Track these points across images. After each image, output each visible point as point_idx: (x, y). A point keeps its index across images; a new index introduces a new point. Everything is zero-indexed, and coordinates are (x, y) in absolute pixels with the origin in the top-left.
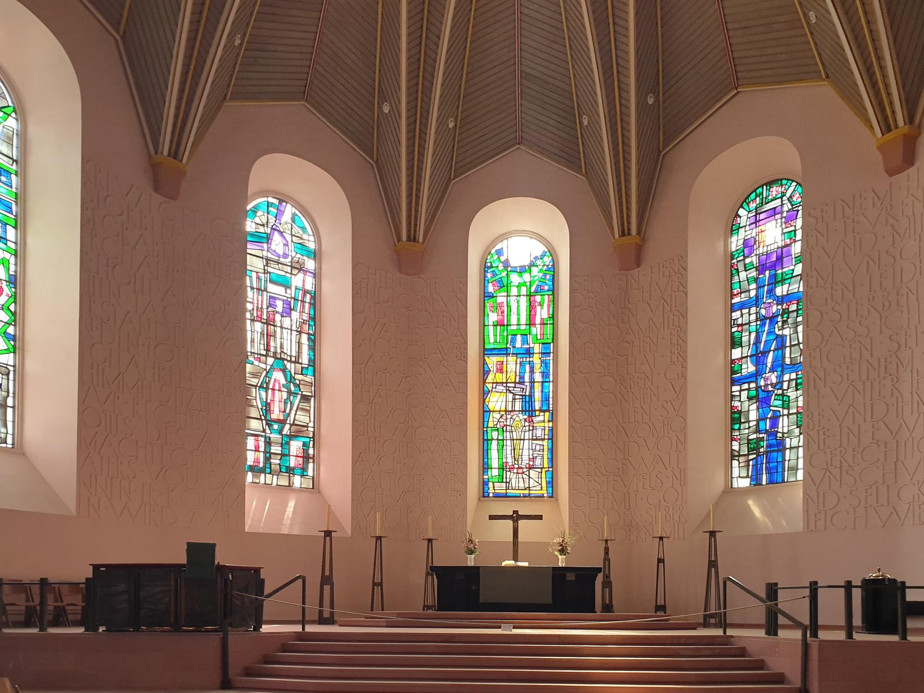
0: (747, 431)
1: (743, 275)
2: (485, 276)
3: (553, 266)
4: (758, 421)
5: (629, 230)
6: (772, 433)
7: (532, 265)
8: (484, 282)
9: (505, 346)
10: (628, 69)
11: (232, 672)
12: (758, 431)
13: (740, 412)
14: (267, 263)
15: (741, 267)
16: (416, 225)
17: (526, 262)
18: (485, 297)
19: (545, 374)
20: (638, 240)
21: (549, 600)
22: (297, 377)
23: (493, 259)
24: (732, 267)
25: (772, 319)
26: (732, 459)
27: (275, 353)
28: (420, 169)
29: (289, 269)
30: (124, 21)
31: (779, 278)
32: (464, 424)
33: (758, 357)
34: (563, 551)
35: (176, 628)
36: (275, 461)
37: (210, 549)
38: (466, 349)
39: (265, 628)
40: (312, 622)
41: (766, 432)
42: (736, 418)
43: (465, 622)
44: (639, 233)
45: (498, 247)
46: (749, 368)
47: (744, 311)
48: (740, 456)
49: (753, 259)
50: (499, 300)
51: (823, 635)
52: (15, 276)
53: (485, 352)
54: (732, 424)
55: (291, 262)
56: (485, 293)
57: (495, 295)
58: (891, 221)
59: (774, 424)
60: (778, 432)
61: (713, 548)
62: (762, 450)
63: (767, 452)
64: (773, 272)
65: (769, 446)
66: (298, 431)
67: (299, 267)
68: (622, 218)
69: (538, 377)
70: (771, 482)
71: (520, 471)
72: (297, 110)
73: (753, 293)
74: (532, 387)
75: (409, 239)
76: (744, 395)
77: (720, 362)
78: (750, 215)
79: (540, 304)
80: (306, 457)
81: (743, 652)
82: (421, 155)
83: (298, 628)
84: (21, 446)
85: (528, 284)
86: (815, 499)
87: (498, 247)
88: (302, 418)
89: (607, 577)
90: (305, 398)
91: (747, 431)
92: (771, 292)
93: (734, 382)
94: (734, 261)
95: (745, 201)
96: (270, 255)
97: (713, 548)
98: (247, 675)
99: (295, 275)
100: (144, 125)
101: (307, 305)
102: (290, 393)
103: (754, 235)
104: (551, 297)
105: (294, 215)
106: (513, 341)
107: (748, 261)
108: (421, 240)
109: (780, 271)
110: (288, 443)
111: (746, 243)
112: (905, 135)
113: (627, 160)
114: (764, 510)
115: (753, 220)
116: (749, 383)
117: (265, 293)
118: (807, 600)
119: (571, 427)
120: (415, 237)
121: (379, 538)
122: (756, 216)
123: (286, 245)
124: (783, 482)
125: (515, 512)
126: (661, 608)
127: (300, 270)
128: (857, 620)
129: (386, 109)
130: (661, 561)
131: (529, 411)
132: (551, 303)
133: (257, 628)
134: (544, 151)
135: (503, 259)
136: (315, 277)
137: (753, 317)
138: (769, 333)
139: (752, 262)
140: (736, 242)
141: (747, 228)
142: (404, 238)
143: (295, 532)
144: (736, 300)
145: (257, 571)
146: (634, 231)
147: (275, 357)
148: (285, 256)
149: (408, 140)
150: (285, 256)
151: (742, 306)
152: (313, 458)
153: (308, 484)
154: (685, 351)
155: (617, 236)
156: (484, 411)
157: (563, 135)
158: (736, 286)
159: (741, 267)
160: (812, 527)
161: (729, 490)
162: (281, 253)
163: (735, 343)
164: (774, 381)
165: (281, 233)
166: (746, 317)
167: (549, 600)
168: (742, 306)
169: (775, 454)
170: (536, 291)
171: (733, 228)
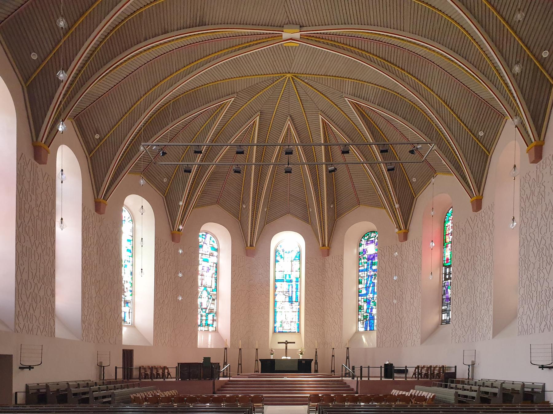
0: (363, 312)
1: (363, 261)
2: (276, 254)
3: (300, 251)
4: (367, 309)
6: (371, 314)
8: (276, 256)
9: (282, 279)
11: (216, 390)
12: (366, 312)
13: (361, 306)
15: (362, 258)
16: (253, 241)
19: (297, 289)
20: (328, 248)
21: (297, 370)
22: (211, 293)
23: (278, 248)
24: (359, 257)
25: (371, 276)
26: (359, 321)
27: (204, 285)
29: (209, 256)
31: (373, 263)
32: (268, 308)
33: (367, 288)
34: (301, 354)
35: (200, 379)
36: (204, 322)
37: (209, 359)
38: (269, 282)
39: (220, 379)
40: (221, 377)
41: (369, 313)
42: (360, 308)
43: (272, 377)
44: (328, 246)
46: (364, 292)
47: (363, 273)
48: (361, 320)
49: (366, 256)
51: (363, 379)
53: (276, 281)
54: (359, 310)
58: (401, 256)
59: (371, 311)
60: (372, 313)
61: (348, 352)
62: (368, 319)
63: (369, 320)
65: (370, 318)
66: (211, 311)
67: (211, 255)
69: (294, 290)
70: (370, 330)
71: (288, 323)
72: (216, 208)
73: (366, 267)
74: (292, 293)
75: (250, 246)
76: (362, 300)
77: (355, 289)
80: (213, 320)
81: (345, 383)
83: (228, 379)
84: (134, 325)
86: (380, 337)
88: (212, 307)
89: (316, 361)
90: (213, 300)
91: (363, 312)
92: (371, 267)
93: (359, 296)
94: (360, 256)
95: (364, 236)
97: (348, 352)
98: (218, 391)
100: (170, 220)
102: (209, 298)
106: (286, 277)
107: (364, 256)
109: (374, 261)
110: (207, 316)
111: (364, 250)
114: (366, 340)
116: (364, 296)
118: (360, 371)
119: (305, 309)
120: (252, 245)
121: (240, 349)
124: (374, 330)
125: (286, 341)
126: (333, 371)
127: (212, 256)
128: (383, 375)
129: (244, 207)
130: (333, 356)
131: (291, 301)
133: (218, 379)
134: (296, 216)
136: (217, 258)
137: (365, 275)
138: (370, 281)
140: (361, 249)
142: (249, 245)
143: (213, 347)
144: (360, 268)
145: (219, 364)
146: (326, 245)
147: (204, 286)
151: (362, 271)
152: (216, 320)
153: (214, 329)
154: (343, 287)
156: (275, 302)
159: (362, 258)
160: (379, 346)
161: (357, 332)
163: (360, 283)
164: (372, 297)
166: (363, 274)
167: (297, 370)
168: (362, 271)
169: (371, 321)
171: (360, 245)
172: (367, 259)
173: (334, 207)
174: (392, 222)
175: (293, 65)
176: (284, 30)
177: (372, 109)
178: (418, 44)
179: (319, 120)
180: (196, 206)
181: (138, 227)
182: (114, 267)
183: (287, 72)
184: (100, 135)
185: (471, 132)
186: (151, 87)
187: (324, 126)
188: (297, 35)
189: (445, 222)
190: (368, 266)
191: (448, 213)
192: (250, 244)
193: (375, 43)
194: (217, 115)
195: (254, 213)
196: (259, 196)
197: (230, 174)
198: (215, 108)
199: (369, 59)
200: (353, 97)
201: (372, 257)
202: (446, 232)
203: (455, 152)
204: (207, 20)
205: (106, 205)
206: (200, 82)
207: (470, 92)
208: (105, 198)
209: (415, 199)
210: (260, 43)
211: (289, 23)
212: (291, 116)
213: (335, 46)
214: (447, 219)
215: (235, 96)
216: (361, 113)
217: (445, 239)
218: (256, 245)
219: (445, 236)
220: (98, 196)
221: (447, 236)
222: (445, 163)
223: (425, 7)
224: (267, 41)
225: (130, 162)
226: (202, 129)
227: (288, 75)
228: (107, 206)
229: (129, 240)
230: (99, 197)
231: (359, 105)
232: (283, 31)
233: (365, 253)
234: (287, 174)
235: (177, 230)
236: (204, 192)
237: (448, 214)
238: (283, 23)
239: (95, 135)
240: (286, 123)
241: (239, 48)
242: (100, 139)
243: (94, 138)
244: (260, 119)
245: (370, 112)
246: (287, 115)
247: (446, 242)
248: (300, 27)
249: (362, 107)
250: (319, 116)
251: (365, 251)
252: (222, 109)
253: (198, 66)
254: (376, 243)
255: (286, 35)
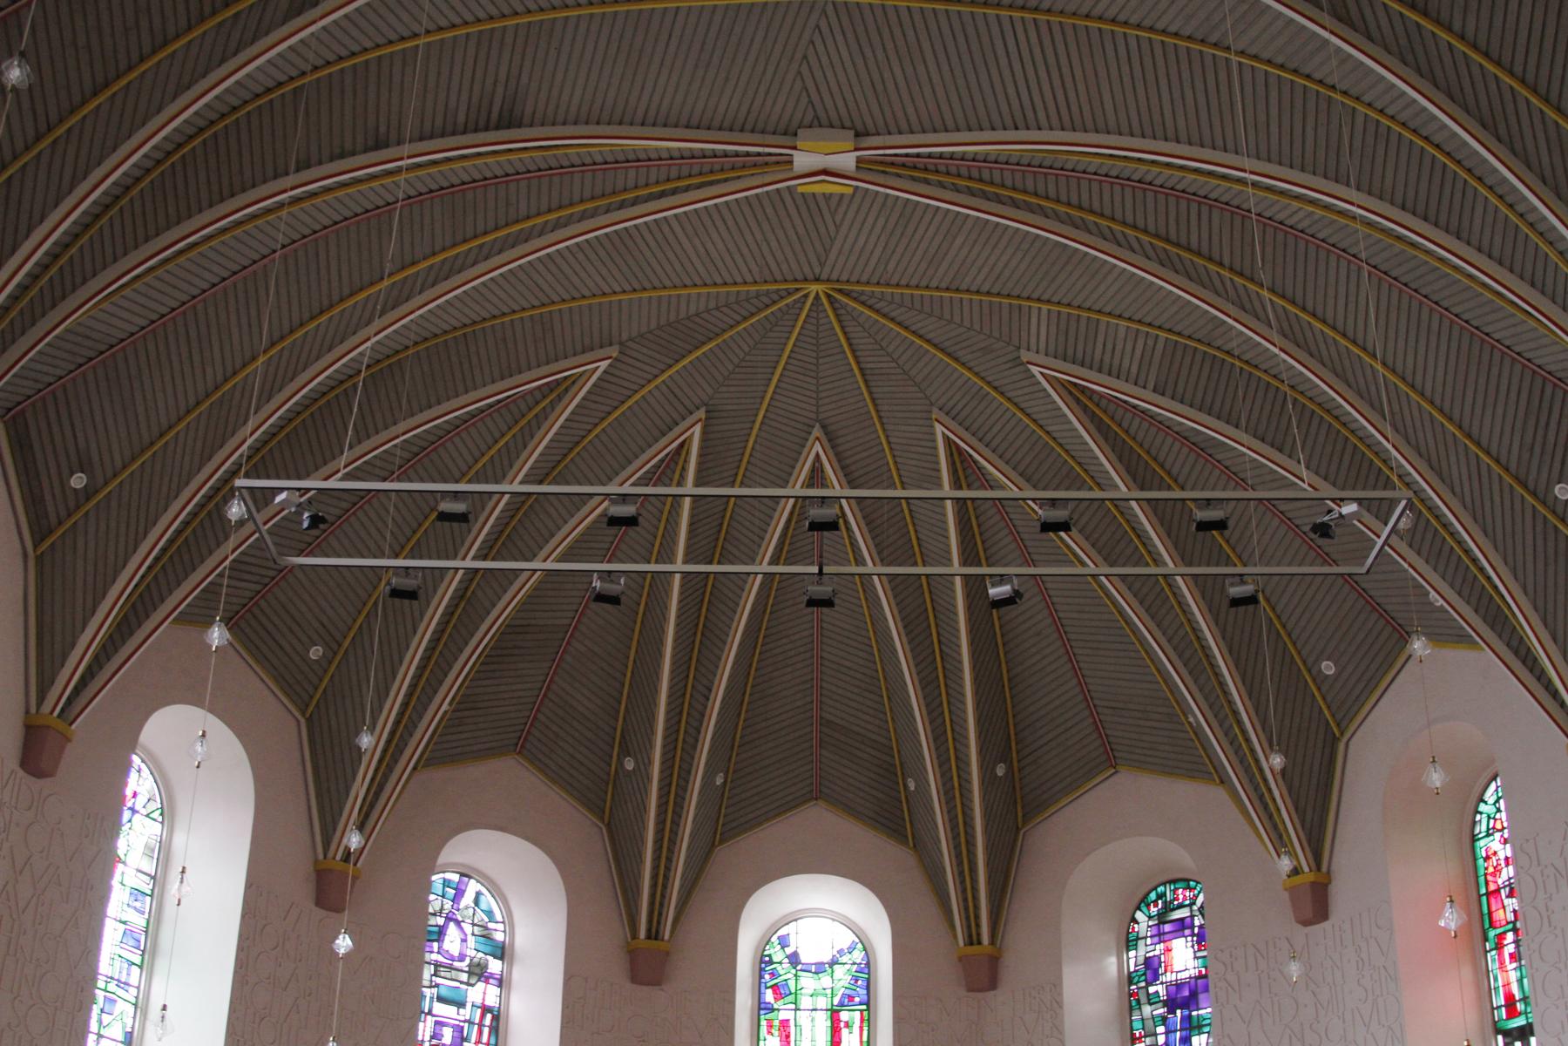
1: (1147, 1009)
3: (868, 964)
5: (979, 935)
7: (833, 963)
10: (966, 738)
14: (436, 971)
15: (1143, 999)
17: (827, 958)
18: (760, 1009)
24: (1131, 995)
28: (672, 842)
29: (464, 977)
30: (314, 702)
31: (1195, 1023)
44: (993, 942)
45: (782, 932)
49: (1159, 989)
50: (783, 1015)
52: (131, 1033)
55: (469, 966)
56: (760, 1003)
57: (776, 1006)
64: (1186, 1012)
67: (478, 972)
68: (968, 918)
75: (649, 937)
78: (1151, 923)
79: (847, 1025)
82: (676, 823)
85: (829, 992)
87: (782, 932)
96: (440, 958)
99: (472, 985)
101: (486, 1031)
103: (1157, 953)
104: (865, 1013)
105: (478, 894)
107: (1152, 989)
108: (667, 937)
109: (1194, 1013)
112: (1313, 883)
113: (971, 844)
115: (1155, 931)
117: (429, 1017)
120: (657, 932)
122: (1158, 925)
123: (464, 941)
132: (865, 1024)
135: (789, 951)
139: (1157, 992)
140: (1133, 959)
141: (1149, 941)
146: (985, 939)
148: (462, 958)
149: (659, 806)
150: (462, 958)
155: (961, 943)
157: (880, 795)
158: (1137, 1025)
159: (1143, 999)
162: (456, 954)
165: (458, 923)
170: (841, 1004)
172: (1165, 1003)
173: (1010, 768)
174: (1248, 830)
175: (832, 256)
176: (799, 144)
177: (1135, 407)
178: (1282, 193)
179: (934, 441)
180: (433, 759)
181: (179, 839)
182: (58, 1004)
183: (810, 276)
184: (91, 477)
185: (1525, 486)
186: (306, 316)
187: (953, 463)
188: (847, 161)
189: (1474, 839)
190: (1171, 1036)
191: (1482, 801)
192: (649, 930)
193: (1027, 174)
194: (543, 416)
195: (671, 775)
196: (695, 724)
197: (623, 546)
198: (529, 398)
199: (1109, 236)
200: (1059, 364)
201: (1186, 993)
202: (1487, 883)
203: (1474, 560)
204: (529, 110)
205: (69, 740)
206: (487, 305)
207: (1493, 347)
208: (69, 712)
209: (1341, 746)
210: (711, 183)
211: (817, 123)
212: (824, 427)
213: (985, 196)
214: (1484, 828)
215: (614, 355)
216: (1093, 417)
217: (1485, 910)
218: (672, 932)
219: (1484, 899)
220: (41, 699)
221: (1493, 900)
222: (1441, 602)
223: (1292, 81)
224: (739, 177)
225: (186, 577)
226: (480, 465)
227: (814, 288)
228: (69, 746)
229: (137, 893)
230: (46, 708)
231: (1083, 389)
232: (795, 148)
233: (1156, 977)
234: (810, 609)
235: (338, 857)
236: (465, 703)
237: (1482, 807)
238: (795, 123)
239: (72, 474)
240: (806, 450)
241: (585, 211)
242: (88, 492)
243: (64, 484)
244: (704, 433)
245: (1137, 420)
246: (811, 423)
247: (1492, 925)
248: (857, 135)
249: (1096, 398)
250: (932, 426)
251: (1152, 968)
252: (560, 398)
253: (485, 251)
254: (1196, 930)
255: (803, 160)
